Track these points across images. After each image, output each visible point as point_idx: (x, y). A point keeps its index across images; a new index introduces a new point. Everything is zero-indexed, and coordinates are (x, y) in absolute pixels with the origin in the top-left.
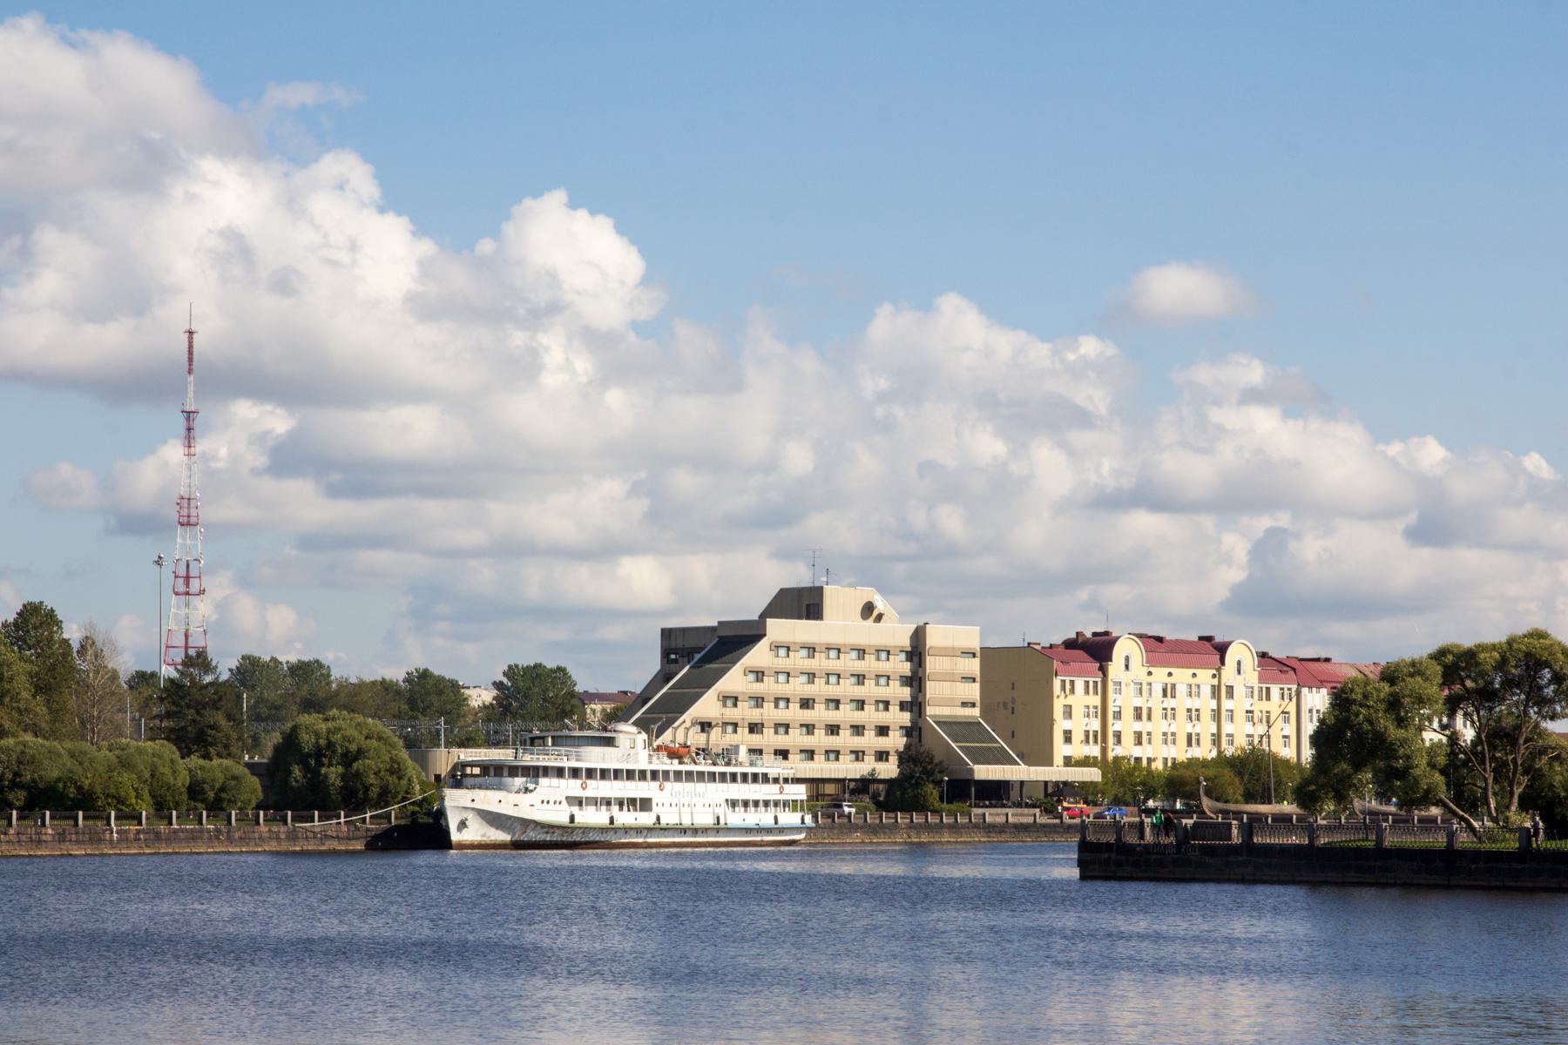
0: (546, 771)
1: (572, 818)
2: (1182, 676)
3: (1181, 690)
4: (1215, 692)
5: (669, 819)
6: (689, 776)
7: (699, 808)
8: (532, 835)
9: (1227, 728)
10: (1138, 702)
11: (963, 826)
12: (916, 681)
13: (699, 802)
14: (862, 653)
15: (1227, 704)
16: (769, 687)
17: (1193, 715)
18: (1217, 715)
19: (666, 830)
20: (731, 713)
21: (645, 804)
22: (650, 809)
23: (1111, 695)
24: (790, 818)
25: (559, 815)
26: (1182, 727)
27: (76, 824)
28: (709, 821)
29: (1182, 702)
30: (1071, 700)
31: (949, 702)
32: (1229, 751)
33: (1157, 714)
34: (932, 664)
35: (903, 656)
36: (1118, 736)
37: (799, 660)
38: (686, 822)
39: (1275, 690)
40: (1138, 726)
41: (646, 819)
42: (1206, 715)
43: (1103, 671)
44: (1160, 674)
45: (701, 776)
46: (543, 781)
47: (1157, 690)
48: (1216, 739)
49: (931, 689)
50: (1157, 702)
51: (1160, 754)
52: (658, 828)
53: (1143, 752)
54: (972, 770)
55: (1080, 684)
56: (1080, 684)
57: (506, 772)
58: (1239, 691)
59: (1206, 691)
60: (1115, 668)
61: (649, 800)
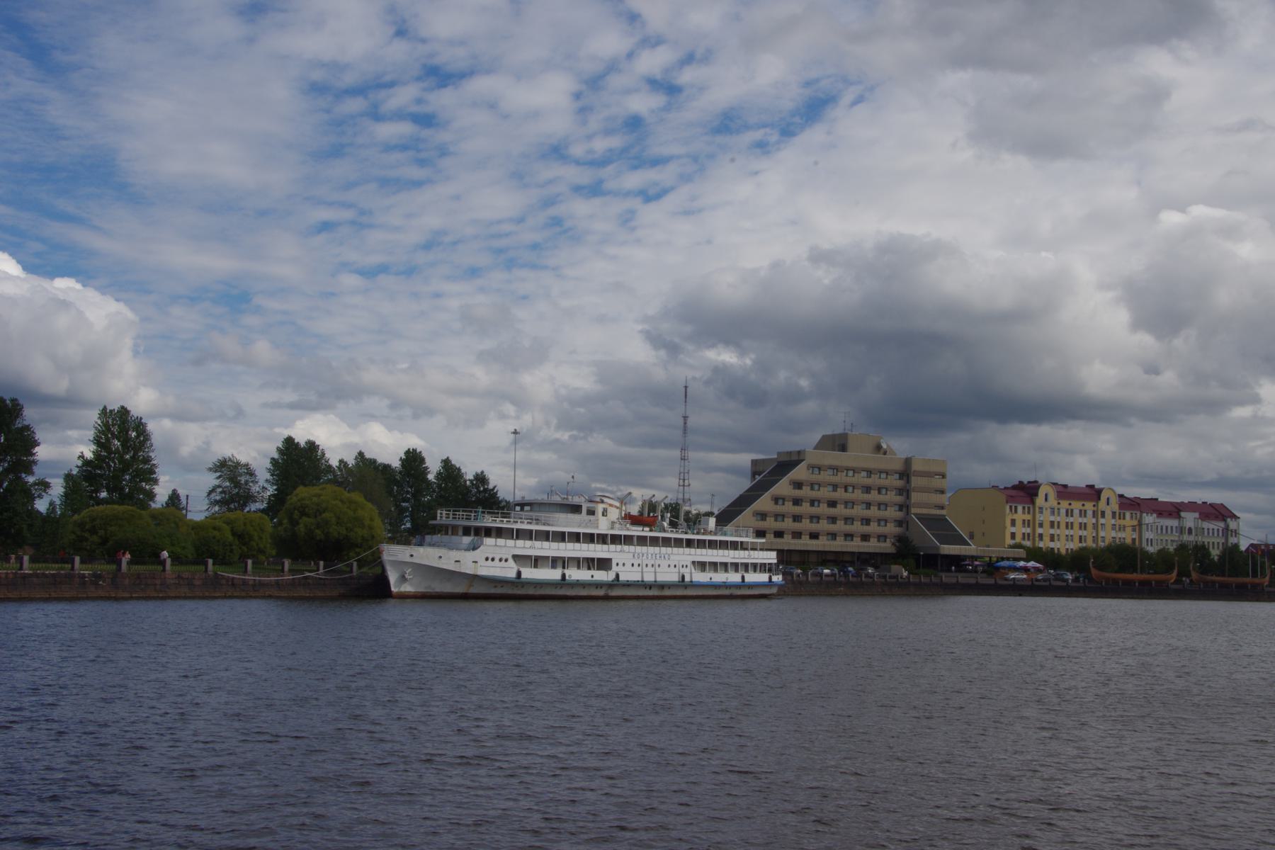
0: (488, 532)
1: (519, 573)
2: (1077, 505)
3: (1076, 512)
4: (1095, 514)
5: (628, 575)
6: (654, 541)
7: (664, 568)
8: (476, 589)
9: (1102, 534)
10: (1052, 518)
11: (925, 584)
12: (905, 491)
13: (664, 563)
14: (870, 472)
15: (1102, 521)
16: (806, 492)
17: (1083, 526)
18: (1095, 526)
19: (628, 585)
20: (779, 508)
21: (604, 564)
22: (610, 568)
23: (1038, 515)
24: (763, 577)
25: (509, 571)
26: (1077, 532)
27: (164, 570)
28: (675, 578)
29: (1076, 519)
30: (1015, 517)
31: (927, 506)
32: (1102, 544)
33: (1063, 525)
34: (916, 481)
35: (897, 476)
36: (1041, 536)
37: (826, 476)
38: (649, 578)
39: (1128, 515)
40: (1052, 531)
41: (600, 576)
42: (1090, 527)
43: (1033, 502)
44: (1065, 504)
45: (667, 542)
46: (489, 541)
47: (1063, 512)
48: (1095, 539)
49: (915, 497)
50: (1062, 518)
51: (1064, 545)
52: (616, 583)
53: (1054, 545)
54: (938, 548)
55: (1020, 508)
56: (1020, 508)
57: (460, 532)
58: (1108, 514)
59: (1090, 513)
60: (1040, 500)
61: (609, 560)
